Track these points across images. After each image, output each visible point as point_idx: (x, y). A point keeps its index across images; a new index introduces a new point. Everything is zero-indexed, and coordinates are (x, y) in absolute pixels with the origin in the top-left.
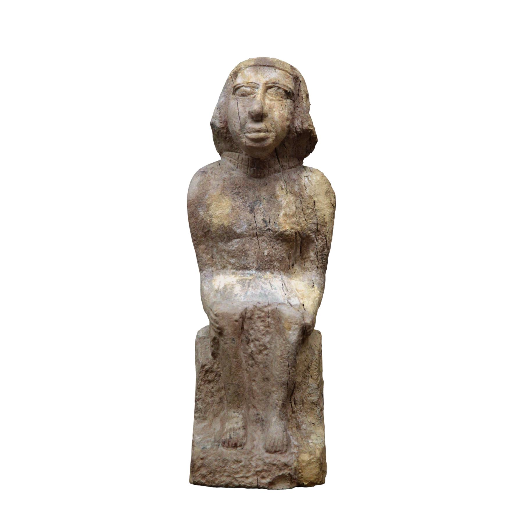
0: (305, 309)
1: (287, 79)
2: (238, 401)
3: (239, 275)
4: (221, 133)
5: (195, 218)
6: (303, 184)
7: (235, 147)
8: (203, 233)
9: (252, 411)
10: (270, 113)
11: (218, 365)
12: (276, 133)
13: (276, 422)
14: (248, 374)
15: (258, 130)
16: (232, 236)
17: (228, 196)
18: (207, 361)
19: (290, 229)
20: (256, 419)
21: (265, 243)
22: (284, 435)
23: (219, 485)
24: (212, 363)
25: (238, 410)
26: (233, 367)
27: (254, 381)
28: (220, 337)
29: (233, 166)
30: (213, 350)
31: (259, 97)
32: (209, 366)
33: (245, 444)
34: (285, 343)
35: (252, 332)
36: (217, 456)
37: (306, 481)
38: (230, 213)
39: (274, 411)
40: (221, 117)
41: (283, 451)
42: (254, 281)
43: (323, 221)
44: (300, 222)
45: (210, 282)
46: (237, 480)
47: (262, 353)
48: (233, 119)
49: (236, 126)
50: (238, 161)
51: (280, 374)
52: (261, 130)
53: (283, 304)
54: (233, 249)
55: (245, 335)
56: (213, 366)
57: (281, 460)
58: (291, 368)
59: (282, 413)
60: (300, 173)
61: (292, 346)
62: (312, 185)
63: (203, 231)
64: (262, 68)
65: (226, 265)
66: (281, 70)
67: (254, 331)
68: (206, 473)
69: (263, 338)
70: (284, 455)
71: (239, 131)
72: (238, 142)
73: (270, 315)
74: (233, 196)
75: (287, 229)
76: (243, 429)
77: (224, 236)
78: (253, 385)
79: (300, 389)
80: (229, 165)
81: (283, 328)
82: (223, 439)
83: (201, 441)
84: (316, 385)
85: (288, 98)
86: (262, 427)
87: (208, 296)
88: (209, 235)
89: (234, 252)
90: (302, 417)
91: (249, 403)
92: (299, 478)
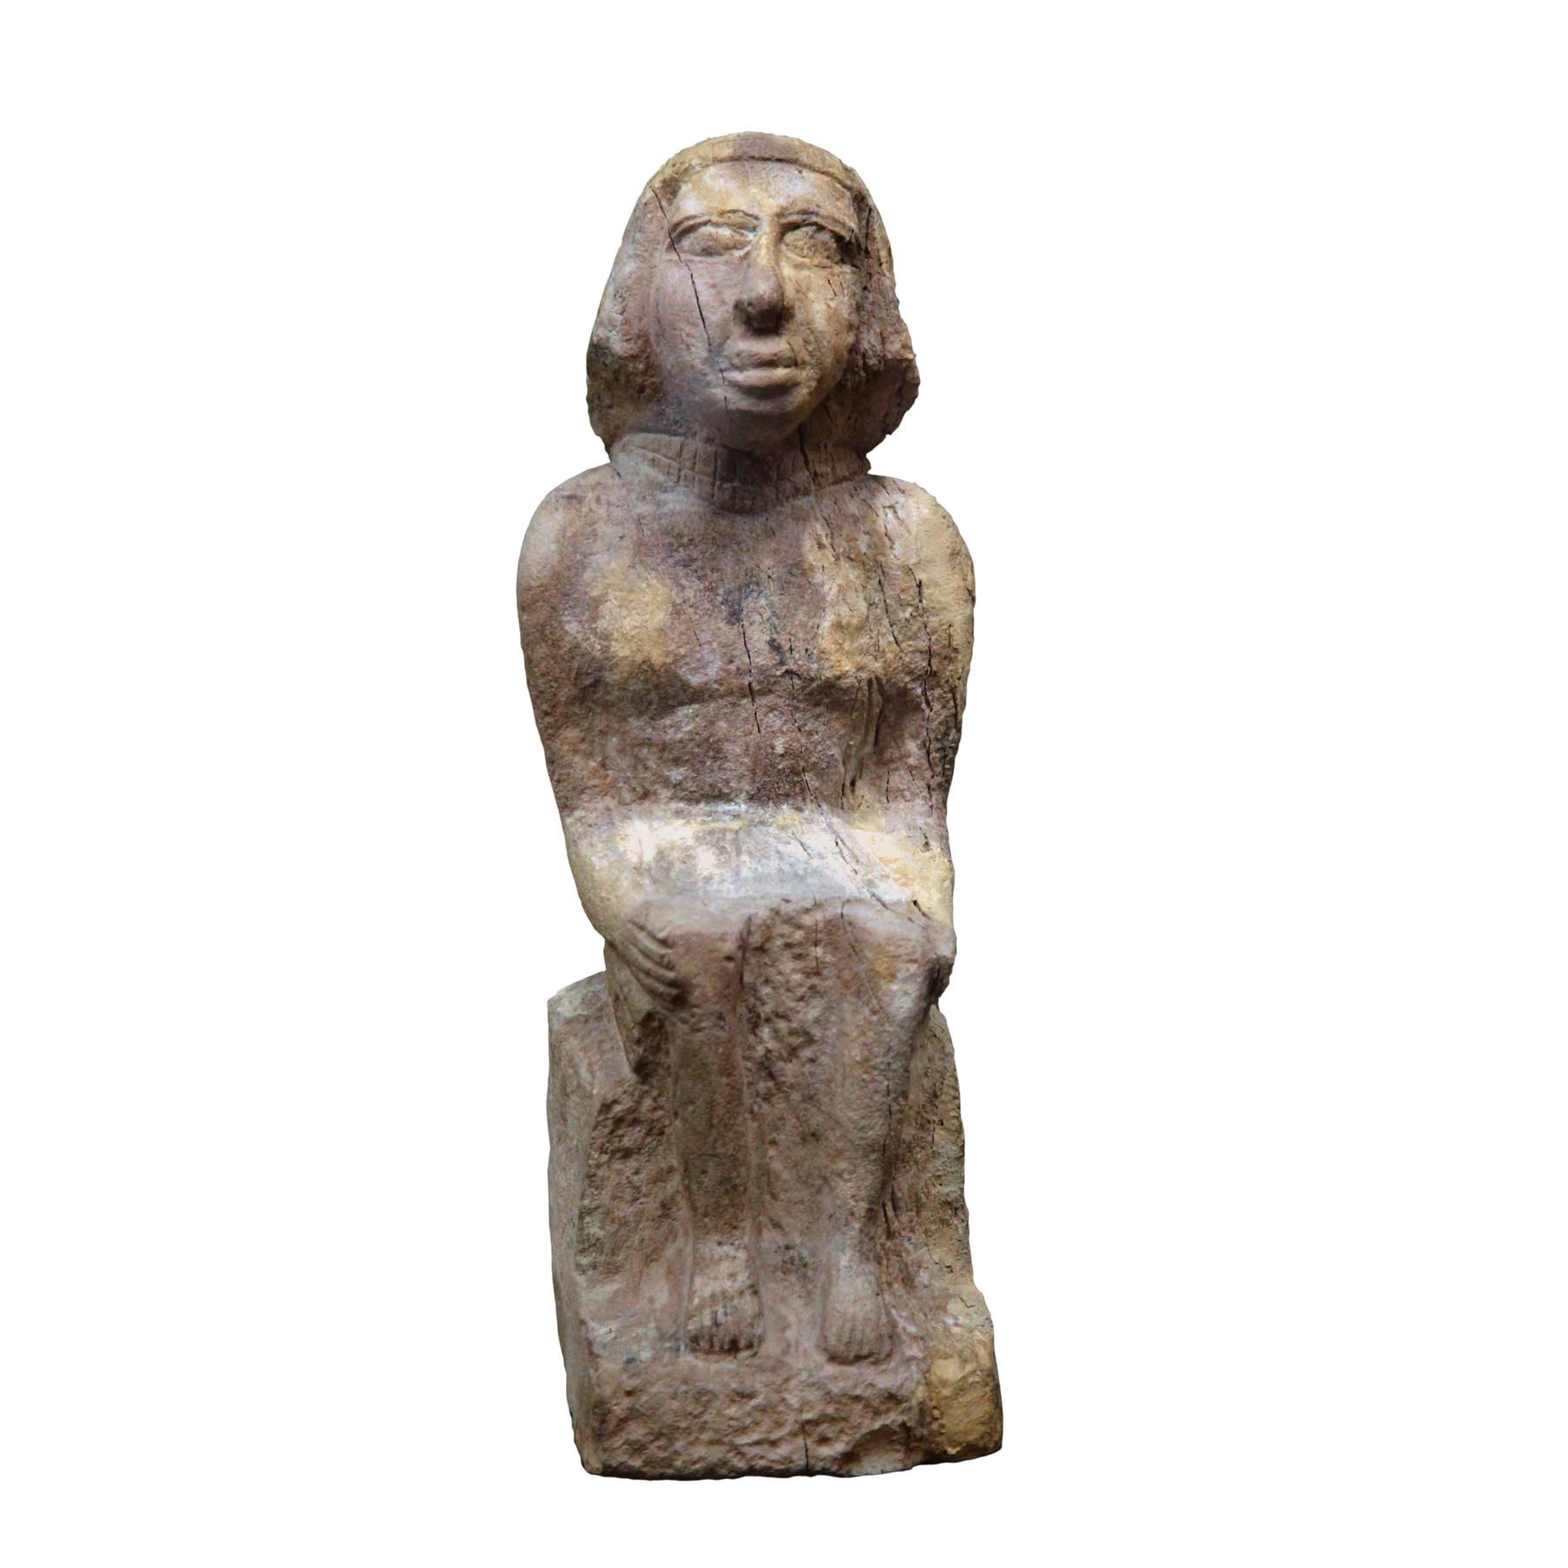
0: (924, 914)
1: (838, 199)
2: (731, 1210)
3: (699, 819)
4: (628, 376)
5: (550, 642)
6: (883, 530)
7: (672, 417)
8: (574, 692)
9: (770, 1238)
10: (799, 308)
11: (655, 1100)
12: (820, 370)
13: (850, 1267)
14: (755, 1125)
15: (770, 358)
16: (675, 697)
17: (657, 571)
18: (620, 1089)
19: (854, 670)
20: (784, 1262)
21: (775, 715)
22: (878, 1307)
23: (687, 1472)
24: (637, 1093)
25: (732, 1236)
26: (719, 1104)
27: (774, 1143)
28: (672, 1011)
29: (661, 478)
30: (641, 1052)
31: (763, 256)
32: (627, 1103)
33: (761, 1340)
34: (879, 1021)
35: (765, 991)
36: (679, 1382)
37: (954, 1444)
38: (669, 624)
39: (843, 1233)
40: (627, 322)
41: (883, 1356)
42: (749, 834)
43: (946, 642)
44: (881, 649)
45: (609, 842)
46: (743, 1454)
47: (797, 1057)
48: (682, 325)
49: (693, 349)
50: (680, 463)
51: (863, 1118)
52: (779, 358)
53: (860, 901)
54: (679, 736)
55: (746, 1000)
56: (639, 1102)
57: (875, 1382)
58: (895, 1100)
59: (867, 1240)
60: (869, 495)
61: (899, 1030)
62: (909, 532)
63: (575, 685)
64: (759, 165)
65: (652, 789)
66: (818, 171)
67: (774, 988)
68: (645, 1436)
69: (799, 1008)
70: (884, 1367)
71: (704, 364)
72: (697, 398)
73: (820, 936)
74: (670, 570)
75: (847, 671)
76: (751, 1295)
77: (649, 697)
78: (771, 1158)
79: (908, 1162)
80: (648, 477)
81: (872, 974)
82: (690, 1328)
83: (615, 1338)
84: (954, 1148)
85: (843, 261)
86: (804, 1286)
87: (611, 886)
88: (596, 696)
89: (681, 745)
90: (916, 1247)
91: (759, 1215)
92: (935, 1436)
